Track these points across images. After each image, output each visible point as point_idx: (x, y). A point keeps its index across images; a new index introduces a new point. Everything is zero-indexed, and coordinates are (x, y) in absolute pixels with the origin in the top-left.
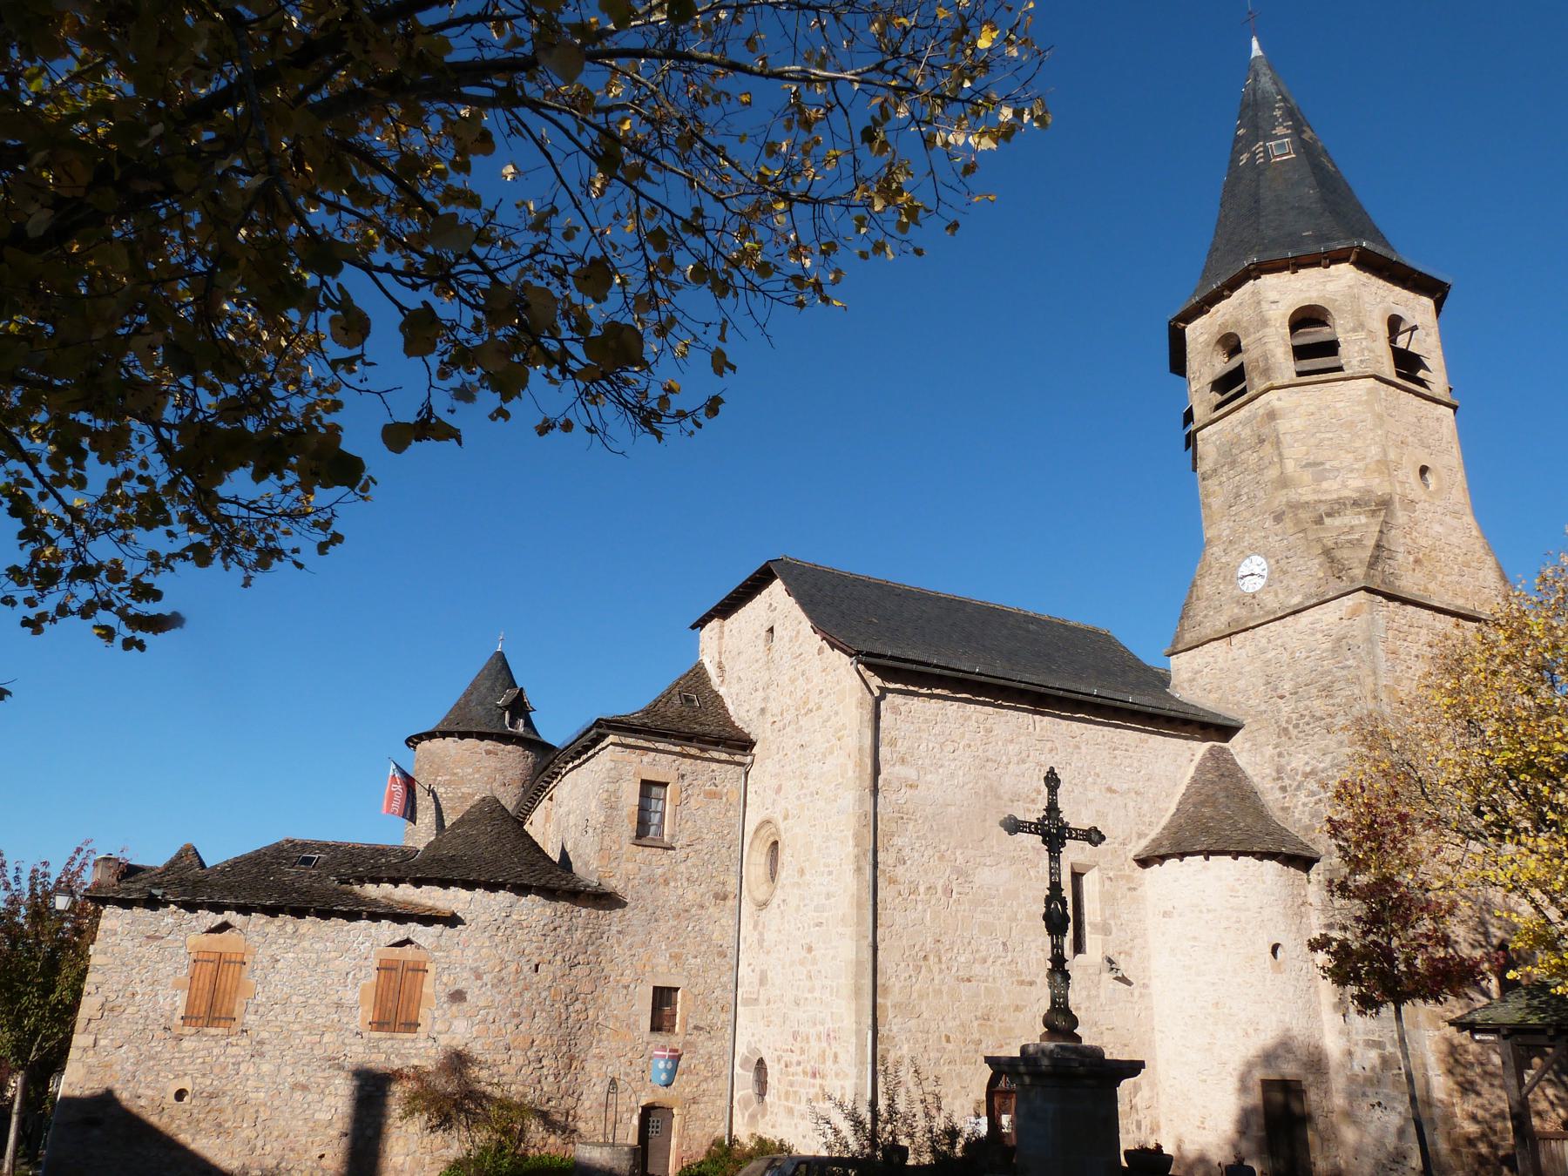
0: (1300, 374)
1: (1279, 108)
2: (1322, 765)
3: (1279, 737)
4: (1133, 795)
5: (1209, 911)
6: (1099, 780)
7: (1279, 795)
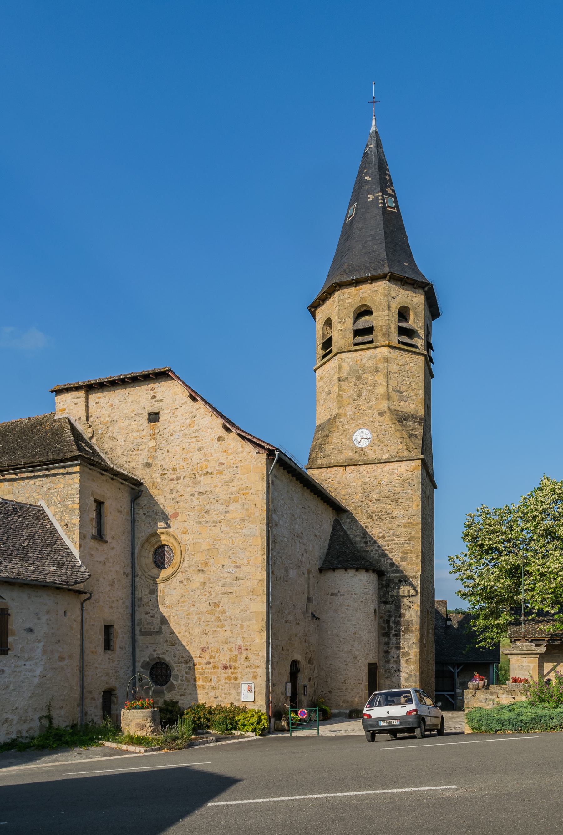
0: (355, 345)
2: (388, 534)
3: (367, 519)
5: (355, 594)
7: (363, 545)
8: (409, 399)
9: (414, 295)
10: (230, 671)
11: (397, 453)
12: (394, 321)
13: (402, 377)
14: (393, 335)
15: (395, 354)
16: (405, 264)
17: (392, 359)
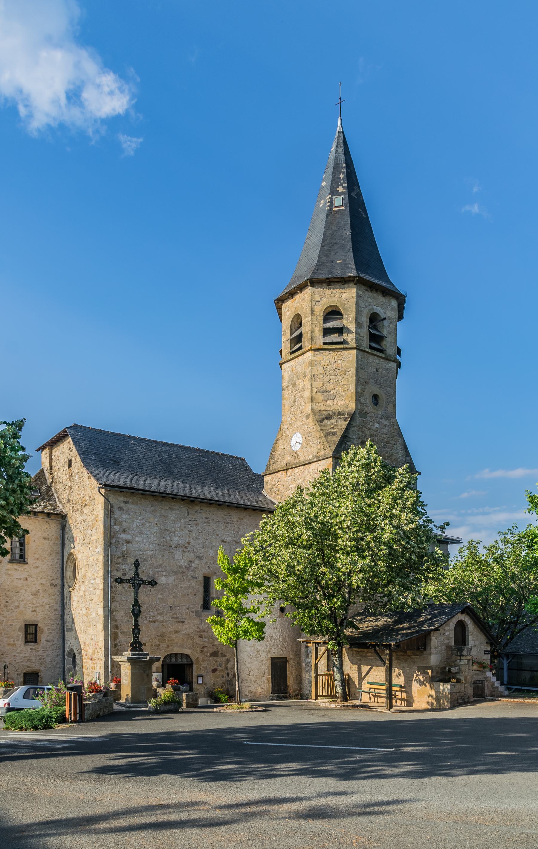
0: (325, 343)
1: (343, 173)
4: (234, 543)
6: (218, 537)
8: (338, 396)
9: (343, 291)
10: (219, 659)
11: (318, 453)
12: (318, 324)
13: (328, 376)
14: (317, 338)
15: (320, 356)
16: (338, 262)
17: (317, 362)
